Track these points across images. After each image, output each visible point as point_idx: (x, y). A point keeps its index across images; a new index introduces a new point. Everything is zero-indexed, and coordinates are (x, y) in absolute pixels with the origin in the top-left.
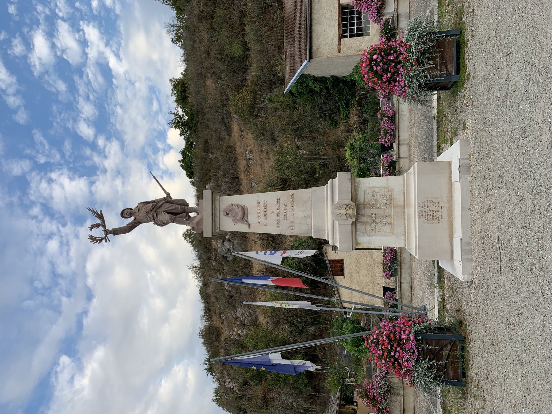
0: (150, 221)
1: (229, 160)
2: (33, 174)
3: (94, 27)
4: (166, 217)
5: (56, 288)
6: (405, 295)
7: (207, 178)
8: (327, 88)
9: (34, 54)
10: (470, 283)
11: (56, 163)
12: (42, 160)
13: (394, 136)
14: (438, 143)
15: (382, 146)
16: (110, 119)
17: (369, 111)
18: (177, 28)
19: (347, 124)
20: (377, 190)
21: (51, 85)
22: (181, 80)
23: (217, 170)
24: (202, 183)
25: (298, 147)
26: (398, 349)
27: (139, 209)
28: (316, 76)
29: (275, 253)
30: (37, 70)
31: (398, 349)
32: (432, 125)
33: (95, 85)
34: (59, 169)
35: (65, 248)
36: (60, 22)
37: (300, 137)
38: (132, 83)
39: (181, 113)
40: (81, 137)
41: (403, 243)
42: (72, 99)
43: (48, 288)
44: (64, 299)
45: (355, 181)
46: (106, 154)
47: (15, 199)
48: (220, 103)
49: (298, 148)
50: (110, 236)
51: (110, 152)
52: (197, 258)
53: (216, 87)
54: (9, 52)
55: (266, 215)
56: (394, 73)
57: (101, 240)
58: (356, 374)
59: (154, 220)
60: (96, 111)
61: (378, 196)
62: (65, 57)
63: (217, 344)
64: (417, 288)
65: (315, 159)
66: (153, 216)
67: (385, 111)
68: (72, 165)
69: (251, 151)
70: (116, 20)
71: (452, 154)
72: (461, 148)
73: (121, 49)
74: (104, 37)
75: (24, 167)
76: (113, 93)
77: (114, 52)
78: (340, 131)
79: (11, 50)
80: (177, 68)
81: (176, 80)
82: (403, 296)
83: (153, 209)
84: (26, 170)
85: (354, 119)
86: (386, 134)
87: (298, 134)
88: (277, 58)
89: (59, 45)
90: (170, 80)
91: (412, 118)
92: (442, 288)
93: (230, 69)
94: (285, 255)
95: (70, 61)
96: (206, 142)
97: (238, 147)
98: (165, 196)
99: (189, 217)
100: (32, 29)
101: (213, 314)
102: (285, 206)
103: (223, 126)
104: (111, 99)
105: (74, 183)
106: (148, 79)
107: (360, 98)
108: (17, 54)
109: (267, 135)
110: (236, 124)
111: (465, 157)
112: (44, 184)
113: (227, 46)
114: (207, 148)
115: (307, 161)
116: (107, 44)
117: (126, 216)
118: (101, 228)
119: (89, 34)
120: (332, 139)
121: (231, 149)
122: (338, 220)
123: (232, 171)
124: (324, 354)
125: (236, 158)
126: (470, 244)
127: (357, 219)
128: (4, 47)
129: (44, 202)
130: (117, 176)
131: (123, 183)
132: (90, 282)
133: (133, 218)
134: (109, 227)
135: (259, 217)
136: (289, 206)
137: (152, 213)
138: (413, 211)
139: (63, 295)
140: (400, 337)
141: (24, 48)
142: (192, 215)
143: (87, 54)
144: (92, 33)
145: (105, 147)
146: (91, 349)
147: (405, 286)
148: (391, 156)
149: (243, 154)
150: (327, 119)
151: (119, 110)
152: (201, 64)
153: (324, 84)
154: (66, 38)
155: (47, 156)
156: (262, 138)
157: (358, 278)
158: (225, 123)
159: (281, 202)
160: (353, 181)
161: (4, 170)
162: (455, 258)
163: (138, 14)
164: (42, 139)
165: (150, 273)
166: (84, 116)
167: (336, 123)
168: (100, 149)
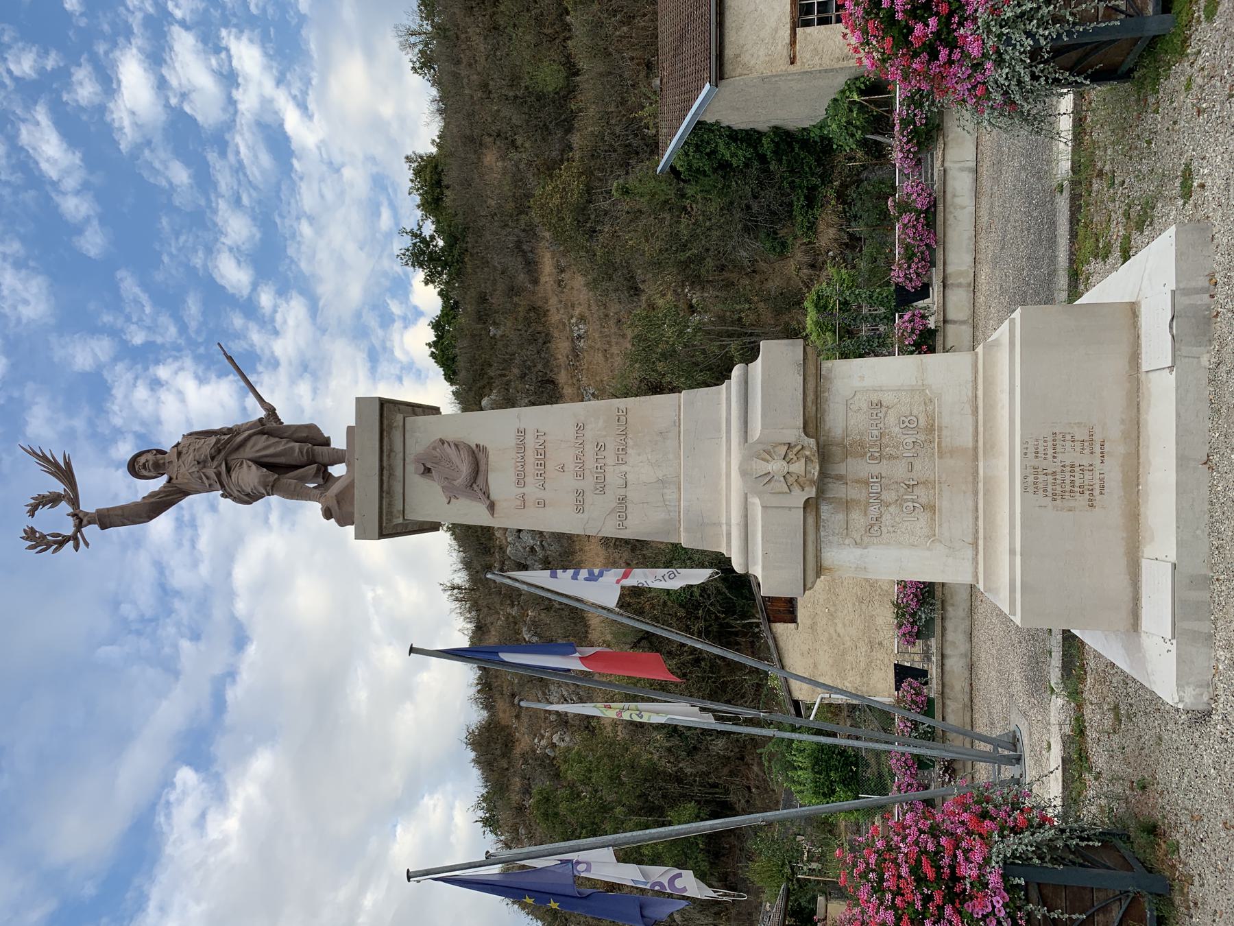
0: (211, 489)
2: (120, 367)
3: (251, 41)
4: (249, 476)
5: (168, 620)
6: (952, 688)
7: (485, 381)
8: (762, 159)
9: (120, 102)
10: (1202, 717)
12: (138, 339)
13: (933, 264)
14: (1072, 262)
15: (900, 289)
17: (865, 216)
18: (423, 37)
19: (810, 248)
20: (887, 399)
21: (157, 172)
22: (431, 158)
23: (507, 363)
24: (472, 394)
25: (691, 306)
26: (948, 911)
27: (179, 454)
28: (735, 128)
29: (601, 574)
30: (127, 138)
31: (948, 911)
32: (1053, 213)
33: (254, 173)
34: (176, 358)
35: (188, 532)
36: (176, 29)
37: (697, 281)
38: (336, 170)
39: (429, 228)
41: (970, 570)
42: (203, 202)
43: (151, 620)
44: (185, 644)
45: (818, 368)
47: (79, 424)
48: (513, 204)
49: (692, 309)
51: (285, 322)
52: (461, 566)
53: (504, 168)
54: (65, 97)
55: (542, 476)
56: (951, 14)
58: (823, 854)
59: (222, 486)
60: (254, 230)
61: (892, 419)
62: (187, 109)
63: (506, 766)
64: (988, 675)
65: (730, 335)
66: (218, 475)
67: (909, 195)
68: (202, 350)
69: (582, 319)
70: (299, 26)
71: (1147, 278)
72: (1180, 255)
73: (310, 92)
74: (274, 64)
75: (99, 354)
76: (293, 190)
77: (294, 97)
78: (793, 266)
79: (69, 93)
80: (424, 132)
81: (421, 157)
82: (947, 690)
83: (219, 451)
84: (102, 359)
85: (828, 235)
86: (909, 258)
88: (644, 90)
89: (174, 82)
90: (407, 158)
91: (984, 213)
92: (1075, 695)
93: (535, 122)
95: (200, 119)
96: (483, 299)
97: (553, 310)
98: (262, 413)
99: (328, 478)
100: (115, 45)
101: (497, 696)
102: (600, 447)
103: (520, 259)
104: (289, 204)
105: (207, 390)
106: (371, 159)
107: (842, 185)
108: (83, 103)
109: (618, 278)
110: (548, 255)
111: (1193, 284)
112: (142, 392)
113: (528, 68)
114: (483, 316)
115: (711, 340)
116: (280, 81)
118: (65, 508)
119: (240, 58)
120: (774, 285)
121: (537, 313)
122: (760, 495)
123: (540, 367)
124: (748, 801)
125: (547, 335)
126: (1205, 582)
127: (821, 492)
128: (55, 86)
129: (143, 431)
130: (301, 376)
131: (315, 391)
133: (165, 478)
134: (89, 505)
135: (521, 481)
136: (611, 446)
137: (215, 463)
138: (1005, 468)
140: (953, 868)
141: (98, 88)
142: (338, 470)
143: (235, 102)
144: (247, 55)
145: (275, 311)
146: (244, 754)
147: (955, 664)
148: (923, 317)
150: (762, 235)
151: (306, 229)
152: (470, 115)
153: (755, 148)
154: (191, 67)
155: (149, 328)
156: (605, 284)
157: (832, 631)
158: (525, 252)
159: (589, 434)
160: (811, 369)
161: (56, 359)
162: (1146, 623)
163: (348, 13)
164: (137, 290)
165: (373, 590)
166: (228, 241)
167: (784, 245)
168: (263, 316)
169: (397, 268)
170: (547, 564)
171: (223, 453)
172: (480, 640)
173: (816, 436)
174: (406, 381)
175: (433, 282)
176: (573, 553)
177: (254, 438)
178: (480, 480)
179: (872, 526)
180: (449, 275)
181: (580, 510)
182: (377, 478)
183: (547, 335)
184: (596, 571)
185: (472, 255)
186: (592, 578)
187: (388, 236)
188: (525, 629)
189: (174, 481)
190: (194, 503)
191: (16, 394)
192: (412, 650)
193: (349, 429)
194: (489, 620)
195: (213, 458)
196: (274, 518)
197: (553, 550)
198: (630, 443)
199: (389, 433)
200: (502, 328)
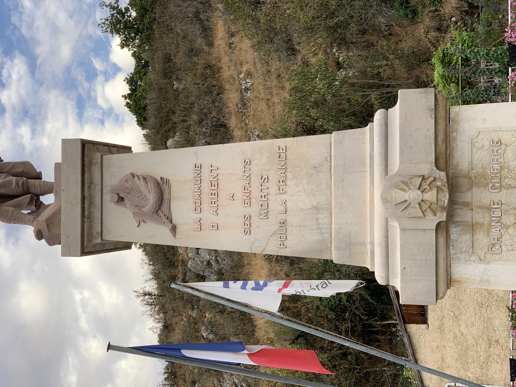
7: (169, 126)
16: (10, 17)
19: (437, 15)
20: (506, 138)
23: (188, 110)
24: (159, 136)
25: (338, 63)
29: (265, 285)
37: (343, 43)
45: (448, 113)
46: (4, 81)
49: (339, 65)
51: (10, 76)
52: (151, 276)
55: (215, 203)
65: (371, 87)
69: (249, 74)
87: (338, 36)
94: (290, 291)
96: (168, 59)
97: (225, 67)
99: (39, 205)
102: (264, 179)
103: (198, 26)
109: (278, 40)
110: (221, 23)
114: (169, 72)
115: (355, 91)
120: (407, 45)
121: (212, 69)
122: (399, 219)
125: (220, 88)
127: (450, 216)
130: (22, 120)
131: (34, 132)
135: (198, 208)
136: (274, 177)
142: (48, 199)
149: (234, 79)
156: (268, 46)
157: (457, 331)
159: (255, 168)
160: (442, 113)
167: (415, 13)
169: (99, 32)
170: (221, 276)
172: (167, 337)
173: (446, 170)
174: (107, 124)
175: (128, 46)
176: (242, 266)
178: (164, 207)
179: (494, 245)
181: (247, 232)
183: (220, 88)
184: (261, 283)
186: (258, 288)
188: (203, 328)
193: (57, 165)
194: (174, 320)
197: (226, 264)
198: (289, 175)
199: (89, 169)
200: (184, 82)
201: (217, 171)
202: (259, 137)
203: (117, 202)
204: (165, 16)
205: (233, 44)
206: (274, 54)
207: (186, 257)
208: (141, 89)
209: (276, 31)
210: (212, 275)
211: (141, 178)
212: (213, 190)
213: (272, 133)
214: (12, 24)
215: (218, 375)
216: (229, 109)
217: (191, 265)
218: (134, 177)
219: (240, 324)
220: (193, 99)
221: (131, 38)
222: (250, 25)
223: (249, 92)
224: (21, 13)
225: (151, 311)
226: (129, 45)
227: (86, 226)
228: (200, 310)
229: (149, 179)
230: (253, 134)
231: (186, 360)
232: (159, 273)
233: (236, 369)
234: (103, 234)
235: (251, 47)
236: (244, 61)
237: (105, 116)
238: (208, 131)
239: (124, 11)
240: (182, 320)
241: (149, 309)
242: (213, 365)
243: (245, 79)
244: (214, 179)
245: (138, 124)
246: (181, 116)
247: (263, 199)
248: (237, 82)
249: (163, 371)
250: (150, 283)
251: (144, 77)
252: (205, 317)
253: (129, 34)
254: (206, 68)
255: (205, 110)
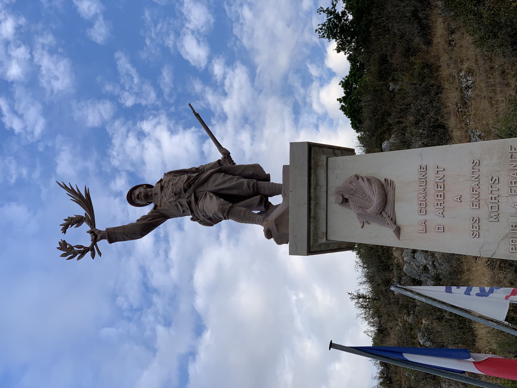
0: (184, 214)
1: (426, 92)
2: (117, 123)
4: (211, 204)
5: (149, 310)
11: (149, 107)
16: (232, 28)
24: (374, 138)
27: (162, 188)
29: (491, 291)
34: (155, 116)
35: (163, 245)
40: (187, 62)
43: (138, 310)
44: (161, 329)
46: (226, 89)
47: (91, 165)
50: (103, 244)
51: (232, 85)
52: (365, 279)
57: (83, 253)
59: (192, 212)
60: (210, 16)
66: (189, 203)
69: (470, 72)
75: (104, 114)
83: (190, 186)
96: (384, 60)
97: (444, 66)
98: (220, 156)
99: (268, 206)
102: (495, 181)
103: (415, 25)
105: (176, 138)
110: (440, 20)
112: (132, 142)
114: (385, 72)
117: (138, 202)
118: (85, 227)
121: (431, 69)
125: (439, 87)
130: (243, 127)
131: (253, 138)
132: (200, 303)
134: (101, 226)
135: (423, 209)
137: (187, 195)
139: (159, 323)
142: (276, 200)
145: (224, 78)
149: (454, 77)
159: (484, 169)
161: (75, 119)
164: (128, 66)
165: (297, 295)
166: (191, 26)
168: (216, 81)
169: (315, 39)
170: (438, 281)
171: (192, 188)
172: (382, 341)
174: (322, 129)
175: (344, 49)
176: (462, 272)
177: (215, 176)
180: (357, 42)
181: (476, 234)
182: (306, 206)
183: (439, 87)
184: (487, 289)
185: (375, 25)
186: (482, 294)
187: (309, 14)
188: (419, 335)
189: (158, 208)
190: (170, 223)
191: (50, 144)
192: (332, 345)
193: (285, 168)
194: (389, 325)
195: (185, 191)
196: (223, 235)
197: (444, 269)
199: (315, 170)
200: (400, 83)
201: (444, 173)
202: (481, 138)
203: (342, 203)
204: (382, 17)
205: (453, 41)
206: (498, 50)
207: (401, 261)
208: (356, 92)
209: (501, 24)
210: (429, 280)
211: (365, 179)
212: (439, 191)
213: (496, 132)
214: (234, 36)
215: (435, 384)
216: (448, 109)
217: (406, 269)
218: (358, 178)
219: (459, 332)
220: (409, 99)
221: (348, 41)
222: (472, 21)
223: (470, 90)
224: (242, 24)
225: (365, 314)
226: (346, 49)
227: (312, 226)
228: (416, 316)
229: (373, 181)
230: (474, 135)
231: (408, 364)
232: (373, 276)
233: (461, 376)
234: (328, 234)
235: (473, 43)
236: (465, 58)
237: (320, 121)
238: (425, 132)
239: (340, 15)
240: (397, 324)
241: (363, 312)
242: (436, 370)
243: (465, 77)
244: (440, 181)
245: (352, 127)
246: (397, 117)
247: (493, 201)
248: (457, 81)
249: (378, 375)
250: (364, 286)
251: (359, 80)
252: (422, 323)
253: (345, 38)
254: (424, 67)
255: (422, 111)
